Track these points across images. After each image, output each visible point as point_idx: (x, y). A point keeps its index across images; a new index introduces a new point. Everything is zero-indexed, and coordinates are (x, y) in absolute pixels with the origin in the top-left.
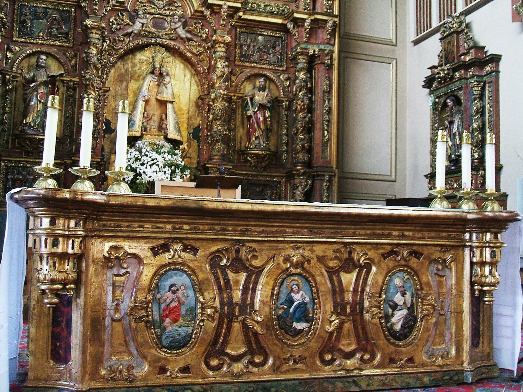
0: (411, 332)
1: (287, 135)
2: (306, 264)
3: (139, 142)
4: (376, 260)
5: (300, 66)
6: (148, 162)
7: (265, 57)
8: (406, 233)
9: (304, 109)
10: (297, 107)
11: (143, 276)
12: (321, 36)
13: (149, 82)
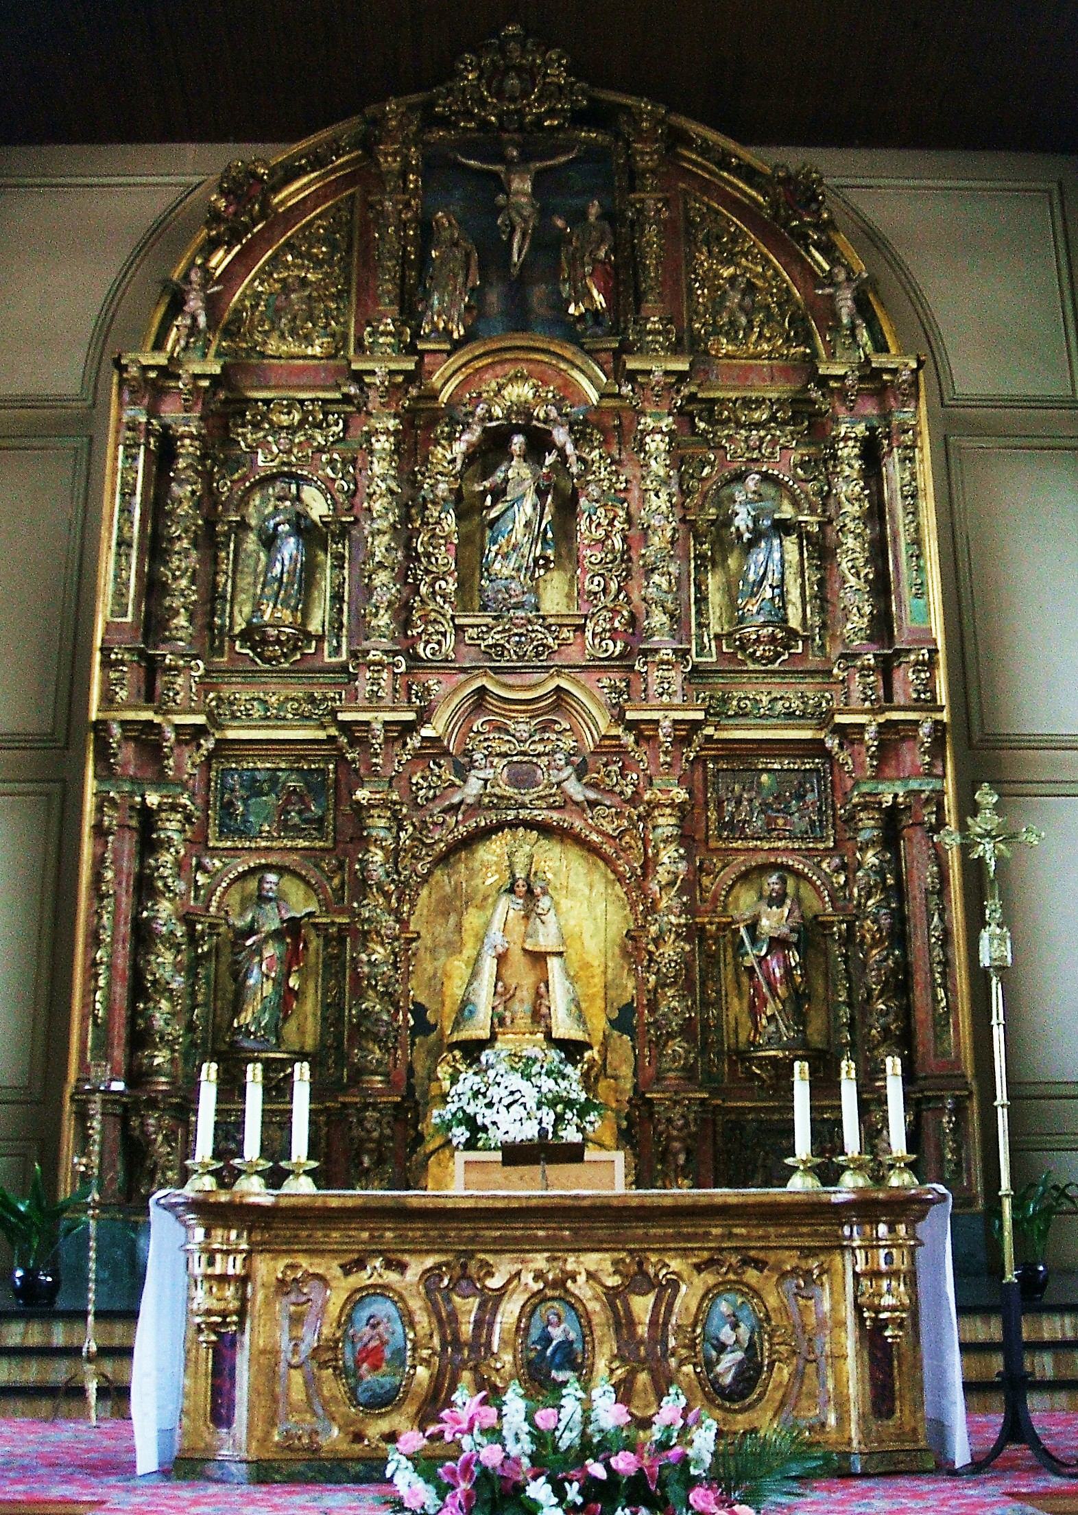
0: (751, 1389)
1: (849, 1005)
2: (569, 1283)
3: (487, 1051)
4: (685, 1274)
5: (864, 836)
7: (780, 822)
8: (737, 1231)
9: (881, 940)
10: (863, 937)
11: (330, 1304)
12: (908, 758)
13: (507, 909)
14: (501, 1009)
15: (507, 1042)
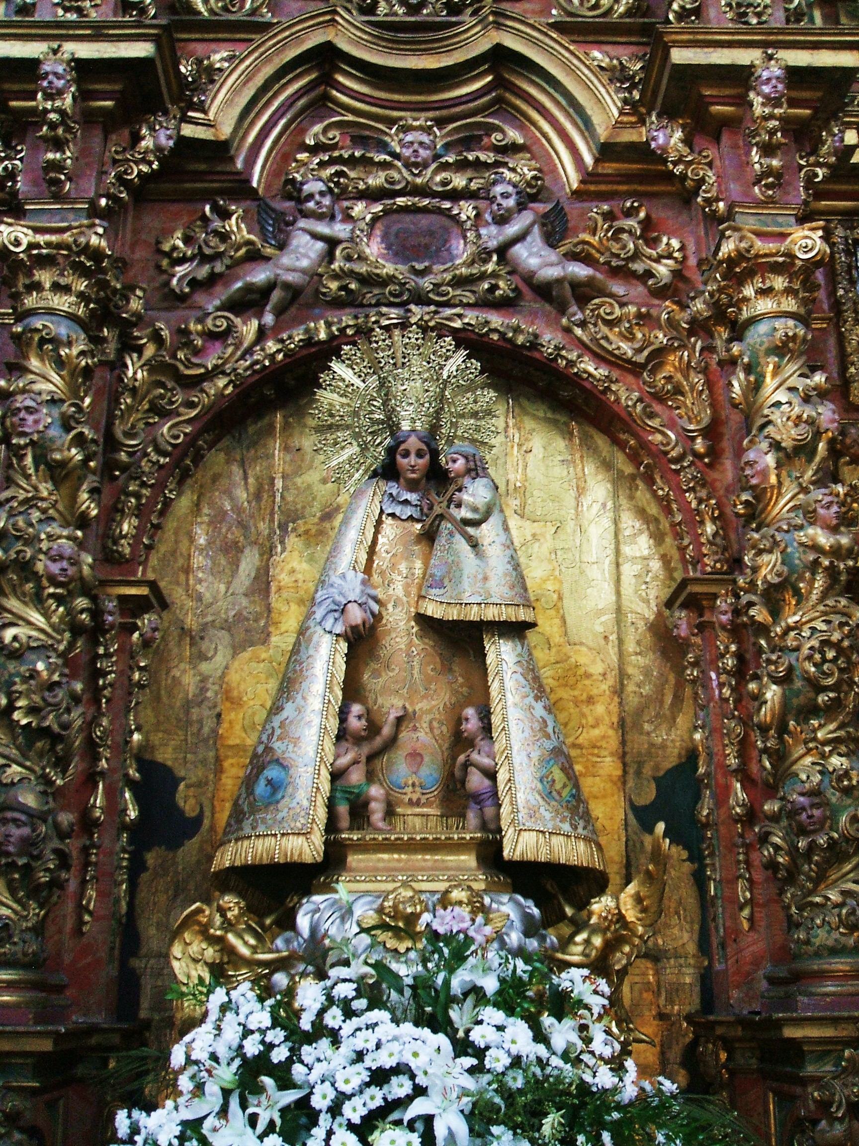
6: (341, 1098)
14: (356, 777)
15: (373, 874)
